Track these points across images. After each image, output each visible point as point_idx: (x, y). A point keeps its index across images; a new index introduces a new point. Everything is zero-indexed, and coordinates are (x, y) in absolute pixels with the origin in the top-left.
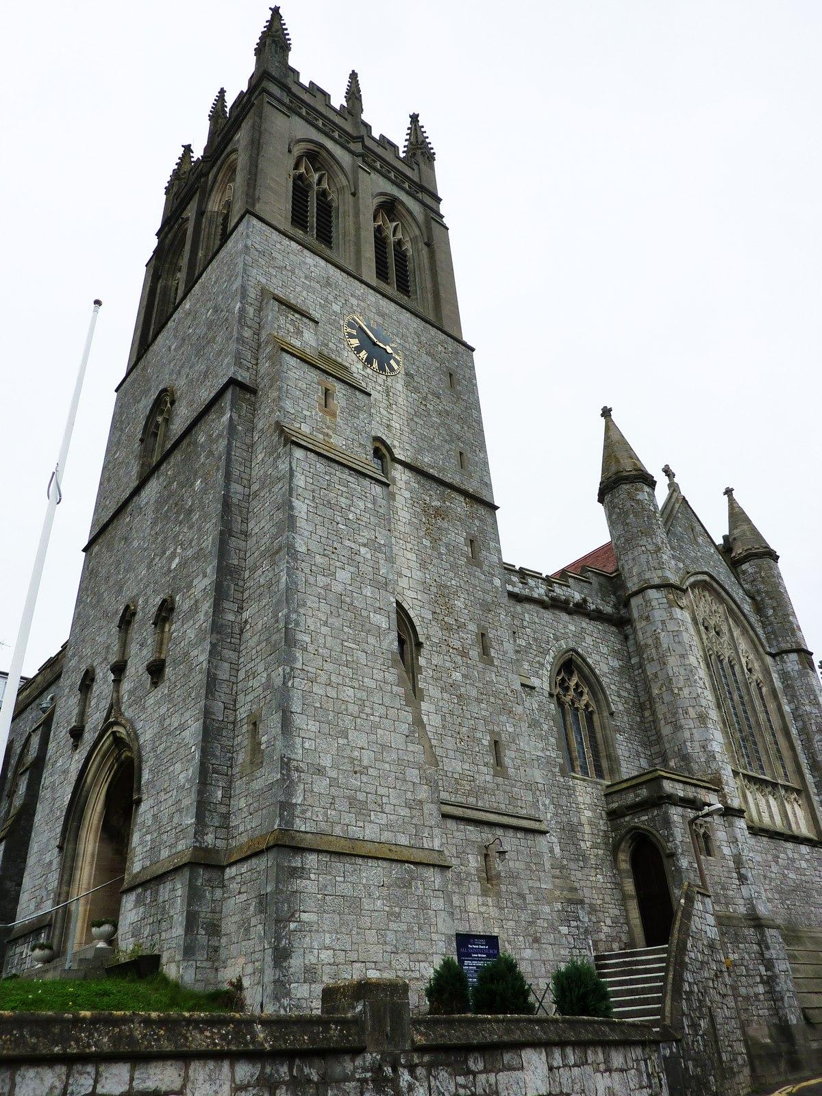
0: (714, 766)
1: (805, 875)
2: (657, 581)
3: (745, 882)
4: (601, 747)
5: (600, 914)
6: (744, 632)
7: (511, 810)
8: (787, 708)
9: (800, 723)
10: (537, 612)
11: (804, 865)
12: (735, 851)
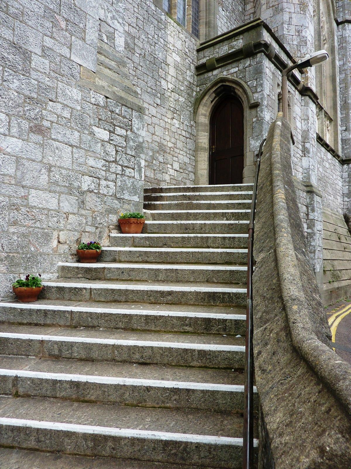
1: (327, 172)
3: (307, 155)
4: (203, 14)
5: (169, 157)
8: (338, 63)
9: (344, 75)
11: (327, 165)
12: (305, 128)
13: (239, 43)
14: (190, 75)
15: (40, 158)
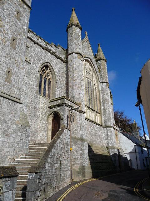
0: (80, 100)
2: (76, 52)
5: (39, 133)
6: (95, 75)
7: (9, 93)
8: (101, 95)
10: (40, 49)
13: (59, 102)
14: (47, 109)
15: (7, 141)
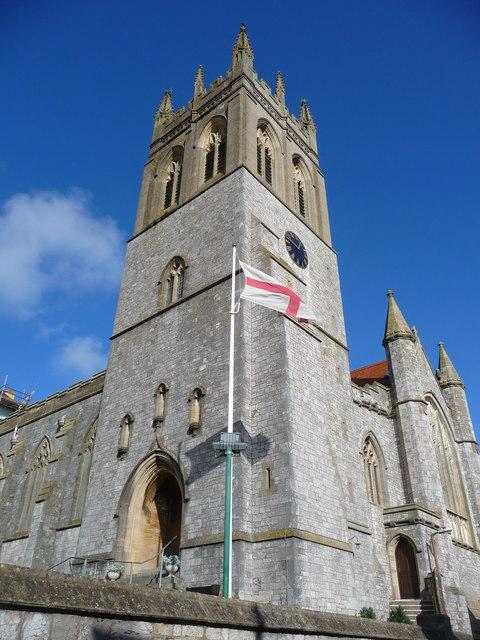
2: (415, 398)
8: (463, 473)
14: (383, 529)
